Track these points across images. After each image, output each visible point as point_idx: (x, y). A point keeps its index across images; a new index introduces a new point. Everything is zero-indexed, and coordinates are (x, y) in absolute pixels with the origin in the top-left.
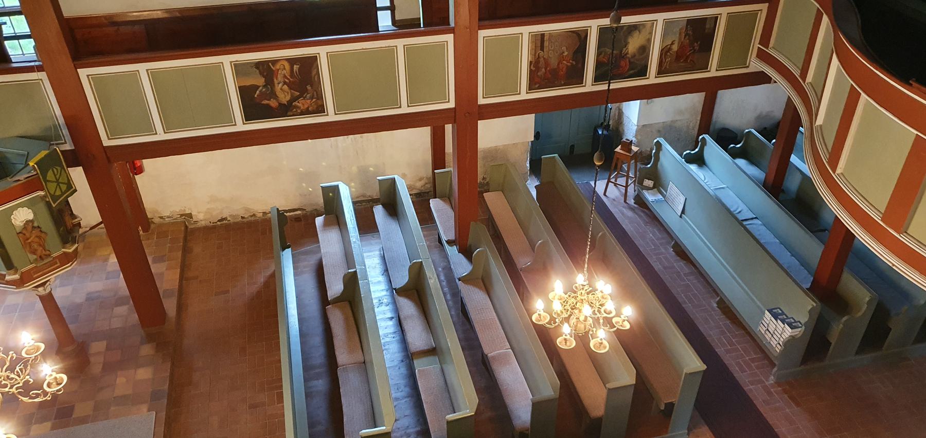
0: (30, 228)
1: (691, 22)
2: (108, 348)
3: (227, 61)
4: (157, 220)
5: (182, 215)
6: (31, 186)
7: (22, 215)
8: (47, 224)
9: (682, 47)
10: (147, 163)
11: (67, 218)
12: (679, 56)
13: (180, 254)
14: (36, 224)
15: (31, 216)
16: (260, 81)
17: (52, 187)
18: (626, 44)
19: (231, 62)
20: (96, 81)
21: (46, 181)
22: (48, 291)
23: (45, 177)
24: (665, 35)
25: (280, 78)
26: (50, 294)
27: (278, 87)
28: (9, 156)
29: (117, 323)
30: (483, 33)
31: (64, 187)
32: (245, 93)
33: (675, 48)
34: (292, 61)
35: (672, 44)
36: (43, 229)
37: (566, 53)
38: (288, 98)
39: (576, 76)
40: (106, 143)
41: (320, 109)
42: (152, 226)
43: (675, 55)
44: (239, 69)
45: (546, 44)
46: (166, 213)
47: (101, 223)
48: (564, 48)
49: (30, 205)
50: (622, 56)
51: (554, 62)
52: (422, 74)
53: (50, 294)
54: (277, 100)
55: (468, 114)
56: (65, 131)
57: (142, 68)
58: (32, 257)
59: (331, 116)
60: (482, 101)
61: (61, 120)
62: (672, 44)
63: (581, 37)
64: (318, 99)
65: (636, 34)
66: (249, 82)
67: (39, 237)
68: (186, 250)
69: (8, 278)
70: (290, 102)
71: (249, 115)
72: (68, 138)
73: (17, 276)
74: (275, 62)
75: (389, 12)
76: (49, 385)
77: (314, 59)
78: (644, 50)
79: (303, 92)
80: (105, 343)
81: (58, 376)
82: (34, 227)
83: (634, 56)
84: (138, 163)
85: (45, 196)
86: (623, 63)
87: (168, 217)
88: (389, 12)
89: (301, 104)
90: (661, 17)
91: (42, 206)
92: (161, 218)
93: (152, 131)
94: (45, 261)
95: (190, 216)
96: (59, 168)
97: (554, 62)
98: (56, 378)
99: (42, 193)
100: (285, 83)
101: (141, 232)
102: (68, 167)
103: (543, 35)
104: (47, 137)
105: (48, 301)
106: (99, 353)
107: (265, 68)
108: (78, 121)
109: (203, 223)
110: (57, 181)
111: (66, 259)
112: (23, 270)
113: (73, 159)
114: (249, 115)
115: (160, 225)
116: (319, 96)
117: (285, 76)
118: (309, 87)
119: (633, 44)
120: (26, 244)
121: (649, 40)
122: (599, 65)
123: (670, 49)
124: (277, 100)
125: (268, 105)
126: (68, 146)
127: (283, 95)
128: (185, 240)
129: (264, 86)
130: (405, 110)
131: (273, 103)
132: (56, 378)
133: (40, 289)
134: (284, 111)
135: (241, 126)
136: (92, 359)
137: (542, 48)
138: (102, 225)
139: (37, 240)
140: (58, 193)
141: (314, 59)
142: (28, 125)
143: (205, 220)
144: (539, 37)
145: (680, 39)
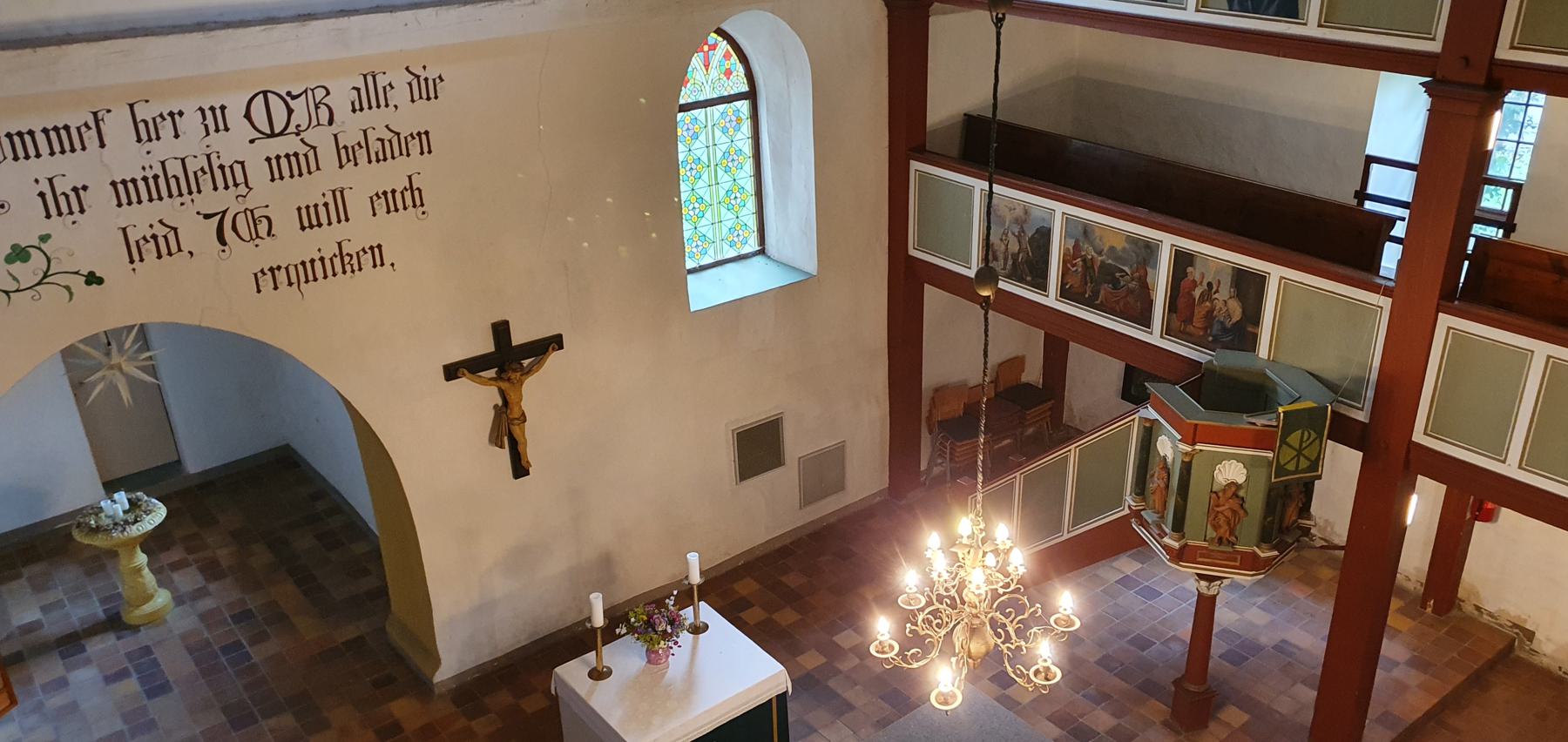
0: (1229, 494)
2: (1244, 728)
4: (1468, 608)
5: (1515, 626)
6: (1261, 440)
7: (1231, 472)
8: (1256, 503)
13: (1461, 678)
14: (1241, 493)
15: (1241, 479)
17: (1288, 454)
19: (1549, 357)
20: (1458, 340)
21: (1283, 442)
22: (1212, 592)
26: (1214, 597)
29: (1284, 706)
31: (1304, 464)
36: (1246, 506)
40: (1418, 437)
42: (1455, 612)
46: (1489, 606)
47: (1342, 548)
53: (1214, 597)
56: (1370, 394)
58: (1211, 533)
61: (1374, 376)
67: (1234, 512)
68: (1478, 681)
69: (1166, 540)
72: (1368, 405)
73: (1176, 545)
75: (1370, 191)
76: (1037, 673)
80: (1246, 717)
81: (1054, 669)
82: (1235, 495)
85: (1270, 464)
87: (1490, 614)
88: (1370, 191)
91: (1262, 474)
92: (1478, 608)
93: (1500, 454)
94: (1222, 548)
95: (1530, 635)
96: (1314, 435)
98: (1048, 669)
101: (1429, 610)
102: (1329, 437)
105: (1206, 606)
106: (1228, 725)
109: (1545, 661)
110: (1299, 452)
111: (1251, 563)
112: (1191, 542)
113: (1345, 432)
115: (1470, 619)
120: (1212, 513)
126: (1362, 416)
128: (1492, 665)
132: (1048, 669)
133: (1203, 583)
136: (1212, 726)
138: (690, 264)
139: (1229, 514)
140: (1291, 467)
142: (1329, 363)
143: (1552, 658)
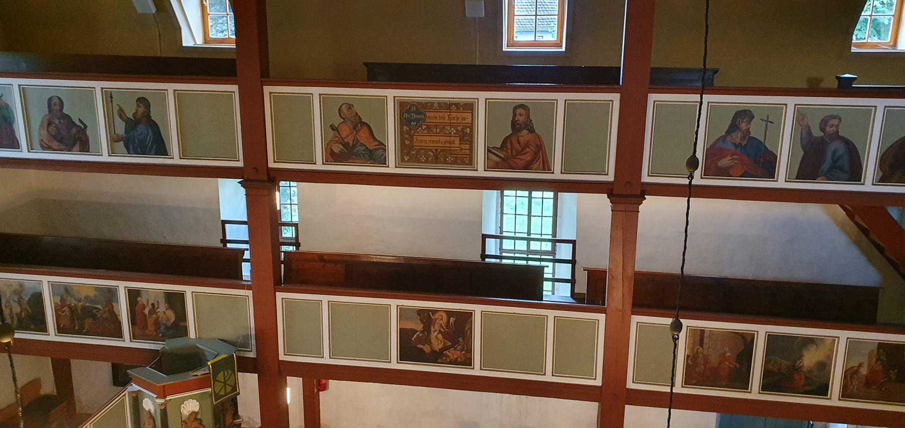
1: (882, 346)
3: (394, 304)
6: (203, 383)
9: (872, 371)
10: (332, 383)
11: (229, 419)
12: (869, 382)
14: (199, 417)
15: (197, 409)
16: (419, 327)
17: (219, 386)
18: (801, 357)
23: (215, 376)
24: (849, 354)
25: (437, 327)
27: (434, 335)
28: (206, 353)
30: (636, 319)
31: (229, 389)
32: (405, 335)
33: (864, 371)
34: (450, 313)
35: (860, 365)
36: (203, 423)
37: (728, 354)
38: (441, 346)
39: (743, 382)
41: (467, 362)
43: (864, 380)
44: (402, 311)
45: (706, 341)
48: (727, 349)
49: (199, 398)
50: (798, 370)
51: (714, 360)
52: (571, 346)
54: (431, 347)
55: (500, 238)
56: (254, 342)
57: (325, 299)
59: (476, 371)
60: (630, 385)
61: (253, 332)
62: (860, 365)
63: (748, 341)
64: (466, 352)
65: (813, 348)
66: (409, 325)
70: (442, 350)
71: (404, 356)
72: (254, 348)
74: (435, 311)
77: (469, 315)
78: (824, 367)
79: (455, 343)
82: (196, 419)
83: (810, 371)
84: (324, 381)
86: (796, 376)
89: (452, 354)
90: (843, 336)
96: (230, 372)
97: (714, 360)
99: (210, 390)
100: (440, 332)
102: (239, 371)
103: (702, 332)
104: (242, 344)
107: (426, 316)
108: (266, 334)
110: (225, 383)
113: (246, 365)
114: (404, 356)
116: (469, 350)
117: (441, 326)
118: (461, 339)
119: (809, 359)
121: (830, 357)
122: (767, 373)
123: (856, 372)
124: (431, 347)
125: (421, 349)
126: (252, 355)
127: (437, 342)
129: (421, 332)
130: (548, 378)
131: (427, 348)
134: (435, 357)
135: (394, 364)
137: (701, 344)
141: (469, 315)
142: (230, 333)
144: (699, 333)
145: (869, 365)
